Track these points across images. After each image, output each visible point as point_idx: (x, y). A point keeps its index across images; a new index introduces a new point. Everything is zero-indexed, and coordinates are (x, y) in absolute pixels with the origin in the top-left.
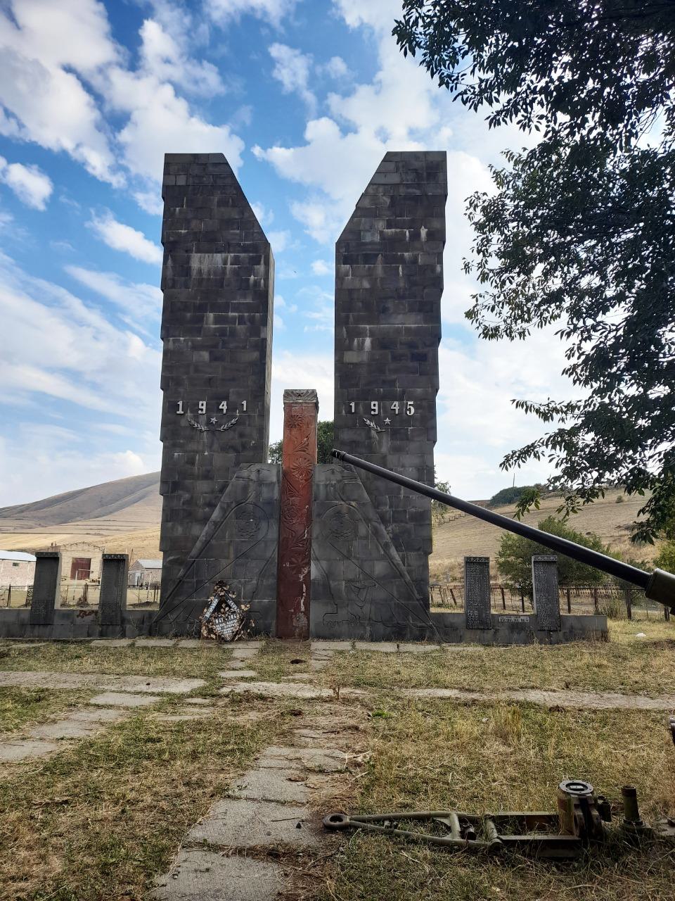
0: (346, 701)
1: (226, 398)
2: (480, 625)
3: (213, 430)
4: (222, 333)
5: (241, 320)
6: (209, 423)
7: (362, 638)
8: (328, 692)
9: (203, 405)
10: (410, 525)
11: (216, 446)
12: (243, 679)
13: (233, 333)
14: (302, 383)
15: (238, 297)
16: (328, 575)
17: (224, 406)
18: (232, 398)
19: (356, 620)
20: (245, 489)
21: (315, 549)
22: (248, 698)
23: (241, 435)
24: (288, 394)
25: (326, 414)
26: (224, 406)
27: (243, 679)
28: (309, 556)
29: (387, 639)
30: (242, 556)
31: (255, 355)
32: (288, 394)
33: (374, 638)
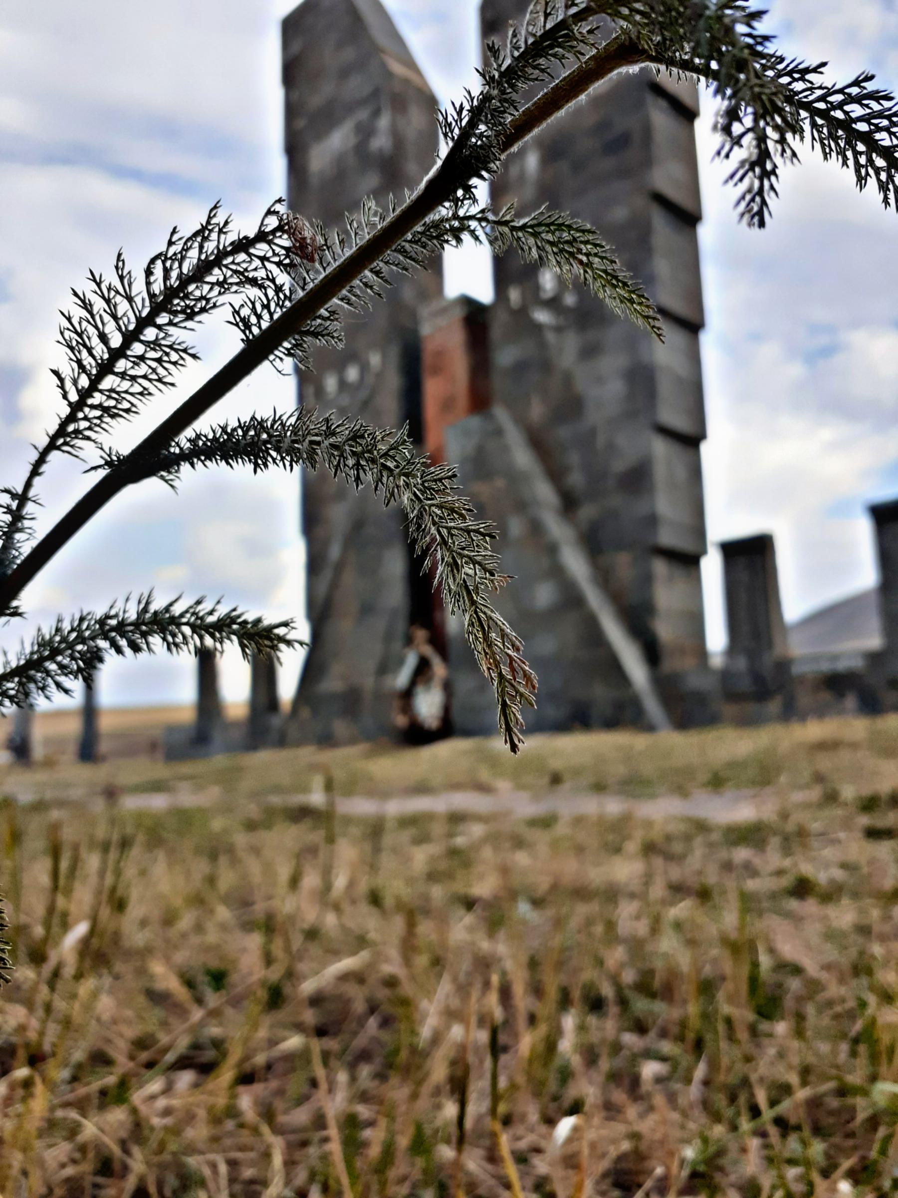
10: (616, 501)
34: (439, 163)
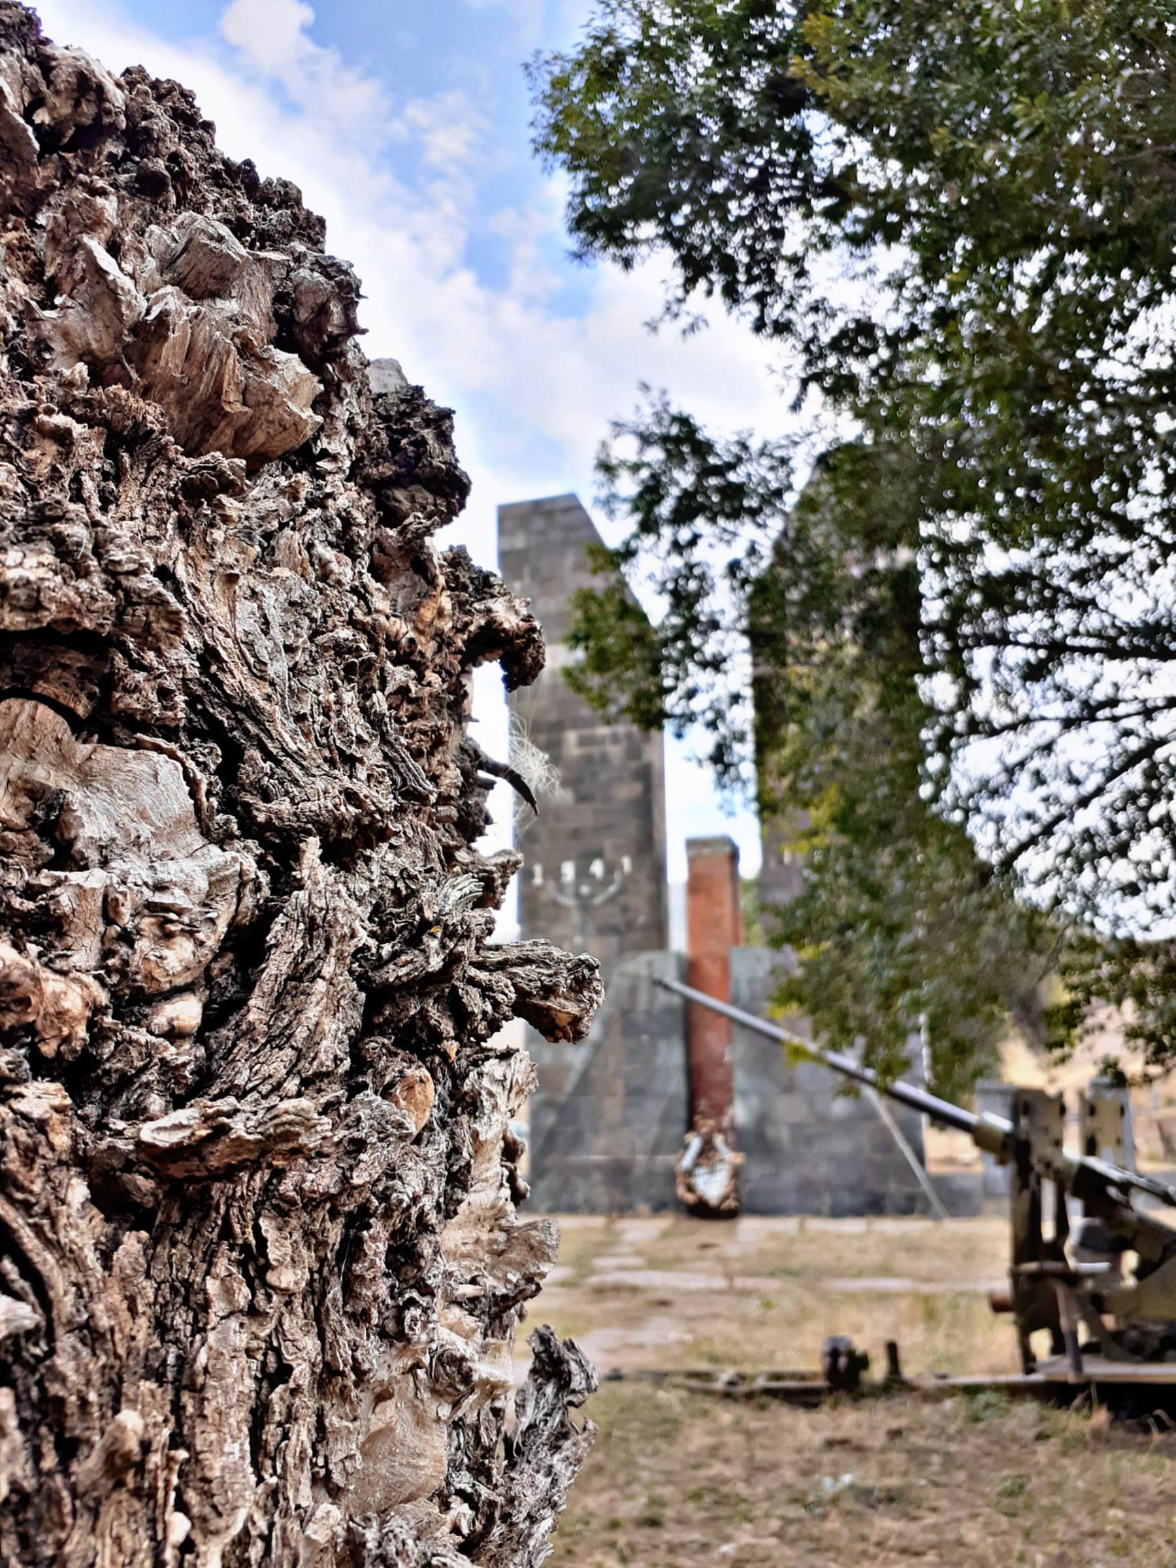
0: (745, 1293)
1: (599, 854)
2: (1148, 1079)
3: (585, 905)
4: (588, 760)
5: (615, 739)
6: (578, 895)
7: (817, 1213)
8: (720, 1283)
9: (569, 870)
11: (591, 928)
12: (623, 1268)
13: (604, 759)
14: (712, 826)
15: (717, 911)
16: (763, 1119)
17: (597, 868)
18: (609, 854)
19: (806, 1187)
20: (633, 991)
21: (740, 1079)
22: (617, 1289)
23: (625, 909)
24: (693, 844)
25: (750, 865)
26: (597, 868)
27: (623, 1268)
28: (729, 1090)
29: (858, 1213)
30: (636, 1093)
31: (636, 788)
32: (693, 844)
33: (837, 1213)
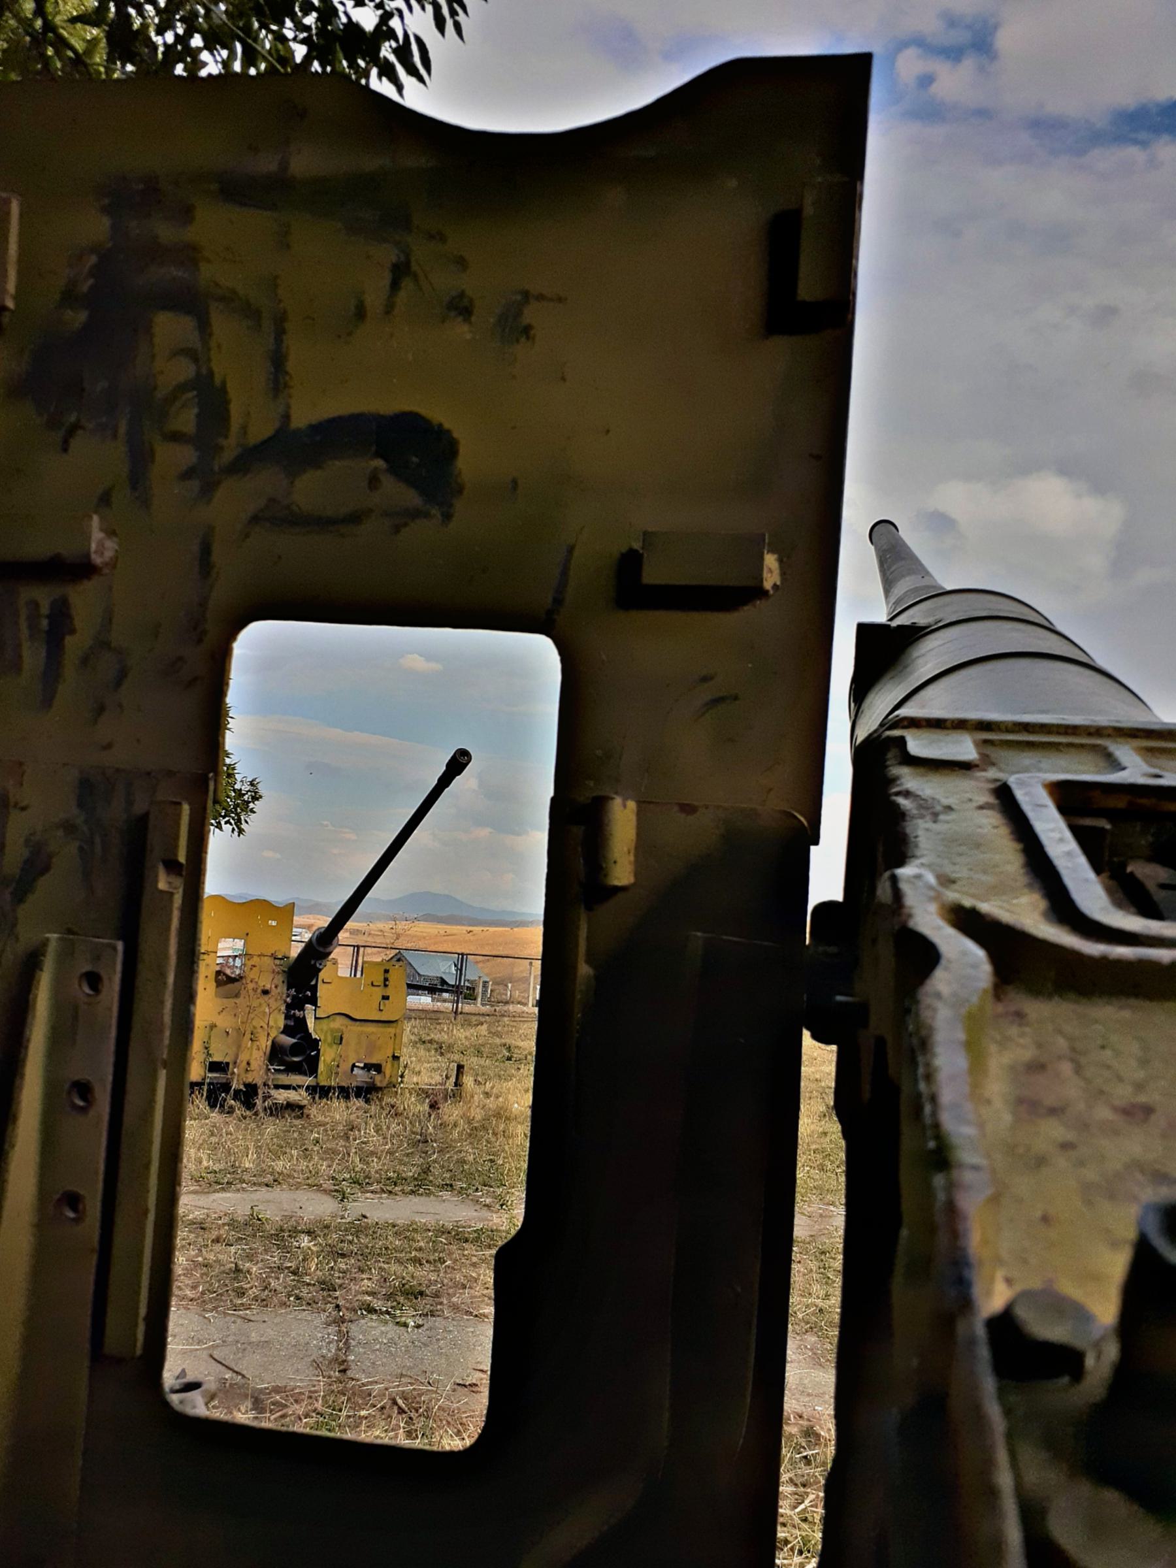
34: (167, 1033)
